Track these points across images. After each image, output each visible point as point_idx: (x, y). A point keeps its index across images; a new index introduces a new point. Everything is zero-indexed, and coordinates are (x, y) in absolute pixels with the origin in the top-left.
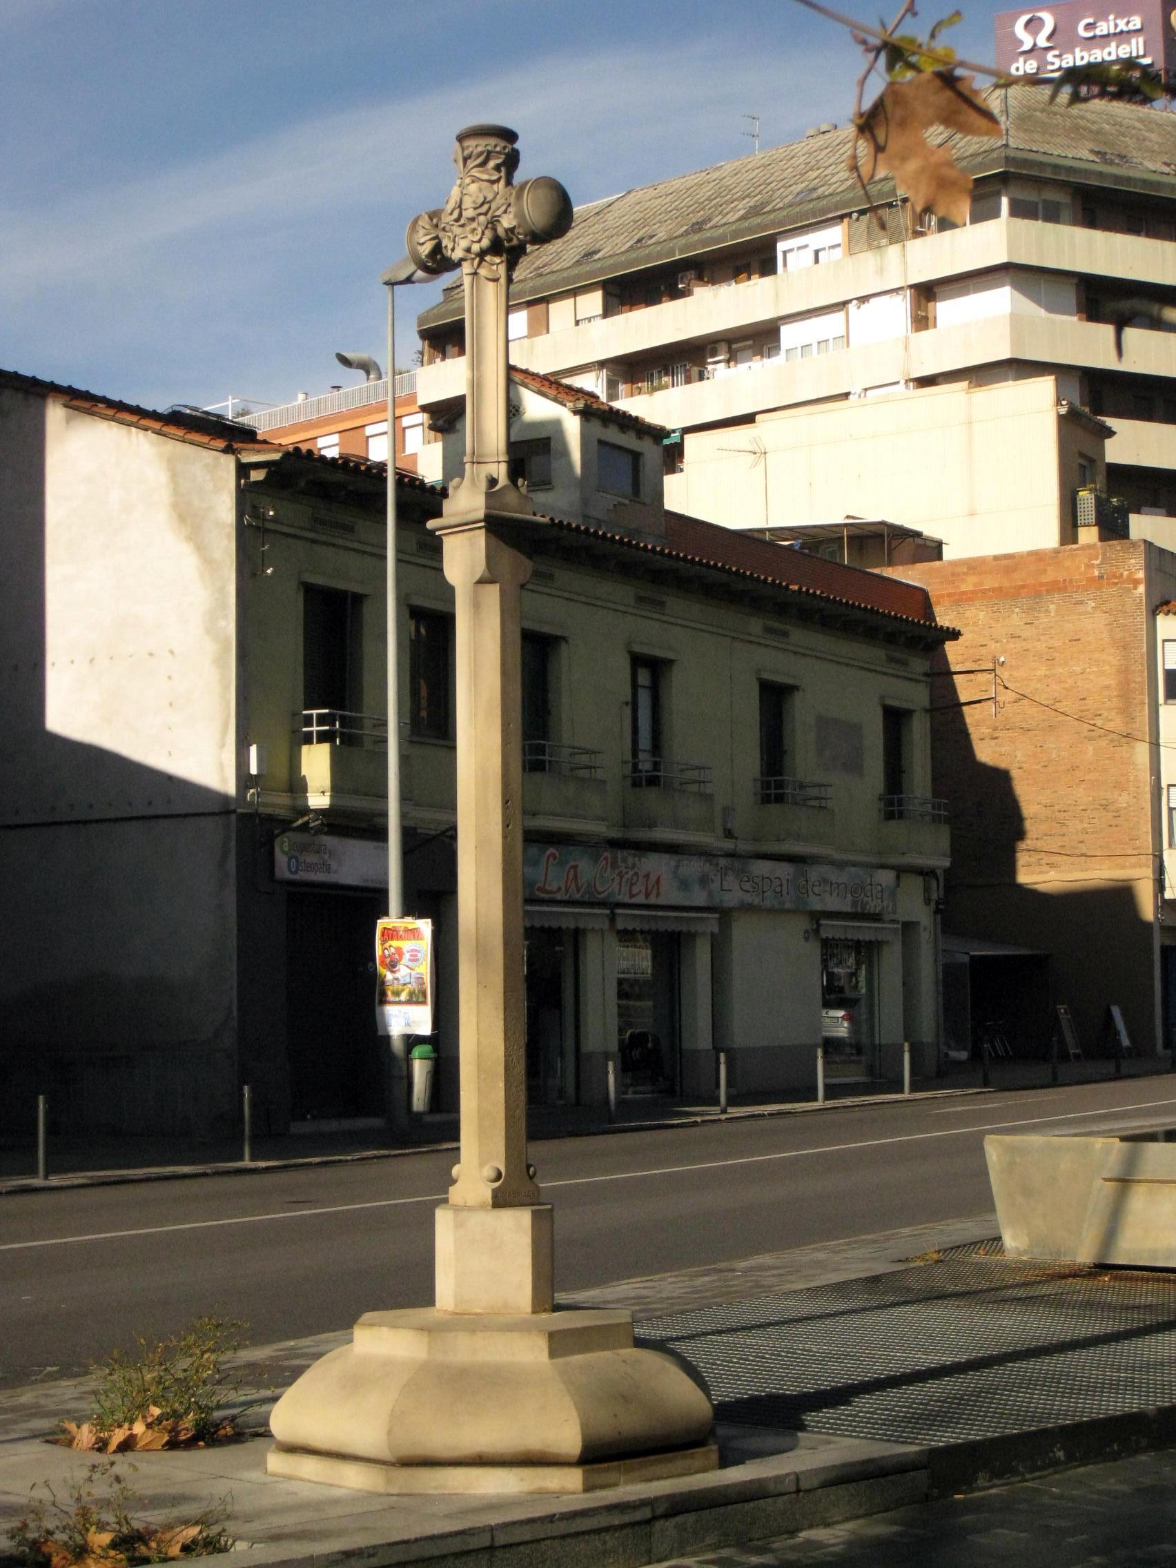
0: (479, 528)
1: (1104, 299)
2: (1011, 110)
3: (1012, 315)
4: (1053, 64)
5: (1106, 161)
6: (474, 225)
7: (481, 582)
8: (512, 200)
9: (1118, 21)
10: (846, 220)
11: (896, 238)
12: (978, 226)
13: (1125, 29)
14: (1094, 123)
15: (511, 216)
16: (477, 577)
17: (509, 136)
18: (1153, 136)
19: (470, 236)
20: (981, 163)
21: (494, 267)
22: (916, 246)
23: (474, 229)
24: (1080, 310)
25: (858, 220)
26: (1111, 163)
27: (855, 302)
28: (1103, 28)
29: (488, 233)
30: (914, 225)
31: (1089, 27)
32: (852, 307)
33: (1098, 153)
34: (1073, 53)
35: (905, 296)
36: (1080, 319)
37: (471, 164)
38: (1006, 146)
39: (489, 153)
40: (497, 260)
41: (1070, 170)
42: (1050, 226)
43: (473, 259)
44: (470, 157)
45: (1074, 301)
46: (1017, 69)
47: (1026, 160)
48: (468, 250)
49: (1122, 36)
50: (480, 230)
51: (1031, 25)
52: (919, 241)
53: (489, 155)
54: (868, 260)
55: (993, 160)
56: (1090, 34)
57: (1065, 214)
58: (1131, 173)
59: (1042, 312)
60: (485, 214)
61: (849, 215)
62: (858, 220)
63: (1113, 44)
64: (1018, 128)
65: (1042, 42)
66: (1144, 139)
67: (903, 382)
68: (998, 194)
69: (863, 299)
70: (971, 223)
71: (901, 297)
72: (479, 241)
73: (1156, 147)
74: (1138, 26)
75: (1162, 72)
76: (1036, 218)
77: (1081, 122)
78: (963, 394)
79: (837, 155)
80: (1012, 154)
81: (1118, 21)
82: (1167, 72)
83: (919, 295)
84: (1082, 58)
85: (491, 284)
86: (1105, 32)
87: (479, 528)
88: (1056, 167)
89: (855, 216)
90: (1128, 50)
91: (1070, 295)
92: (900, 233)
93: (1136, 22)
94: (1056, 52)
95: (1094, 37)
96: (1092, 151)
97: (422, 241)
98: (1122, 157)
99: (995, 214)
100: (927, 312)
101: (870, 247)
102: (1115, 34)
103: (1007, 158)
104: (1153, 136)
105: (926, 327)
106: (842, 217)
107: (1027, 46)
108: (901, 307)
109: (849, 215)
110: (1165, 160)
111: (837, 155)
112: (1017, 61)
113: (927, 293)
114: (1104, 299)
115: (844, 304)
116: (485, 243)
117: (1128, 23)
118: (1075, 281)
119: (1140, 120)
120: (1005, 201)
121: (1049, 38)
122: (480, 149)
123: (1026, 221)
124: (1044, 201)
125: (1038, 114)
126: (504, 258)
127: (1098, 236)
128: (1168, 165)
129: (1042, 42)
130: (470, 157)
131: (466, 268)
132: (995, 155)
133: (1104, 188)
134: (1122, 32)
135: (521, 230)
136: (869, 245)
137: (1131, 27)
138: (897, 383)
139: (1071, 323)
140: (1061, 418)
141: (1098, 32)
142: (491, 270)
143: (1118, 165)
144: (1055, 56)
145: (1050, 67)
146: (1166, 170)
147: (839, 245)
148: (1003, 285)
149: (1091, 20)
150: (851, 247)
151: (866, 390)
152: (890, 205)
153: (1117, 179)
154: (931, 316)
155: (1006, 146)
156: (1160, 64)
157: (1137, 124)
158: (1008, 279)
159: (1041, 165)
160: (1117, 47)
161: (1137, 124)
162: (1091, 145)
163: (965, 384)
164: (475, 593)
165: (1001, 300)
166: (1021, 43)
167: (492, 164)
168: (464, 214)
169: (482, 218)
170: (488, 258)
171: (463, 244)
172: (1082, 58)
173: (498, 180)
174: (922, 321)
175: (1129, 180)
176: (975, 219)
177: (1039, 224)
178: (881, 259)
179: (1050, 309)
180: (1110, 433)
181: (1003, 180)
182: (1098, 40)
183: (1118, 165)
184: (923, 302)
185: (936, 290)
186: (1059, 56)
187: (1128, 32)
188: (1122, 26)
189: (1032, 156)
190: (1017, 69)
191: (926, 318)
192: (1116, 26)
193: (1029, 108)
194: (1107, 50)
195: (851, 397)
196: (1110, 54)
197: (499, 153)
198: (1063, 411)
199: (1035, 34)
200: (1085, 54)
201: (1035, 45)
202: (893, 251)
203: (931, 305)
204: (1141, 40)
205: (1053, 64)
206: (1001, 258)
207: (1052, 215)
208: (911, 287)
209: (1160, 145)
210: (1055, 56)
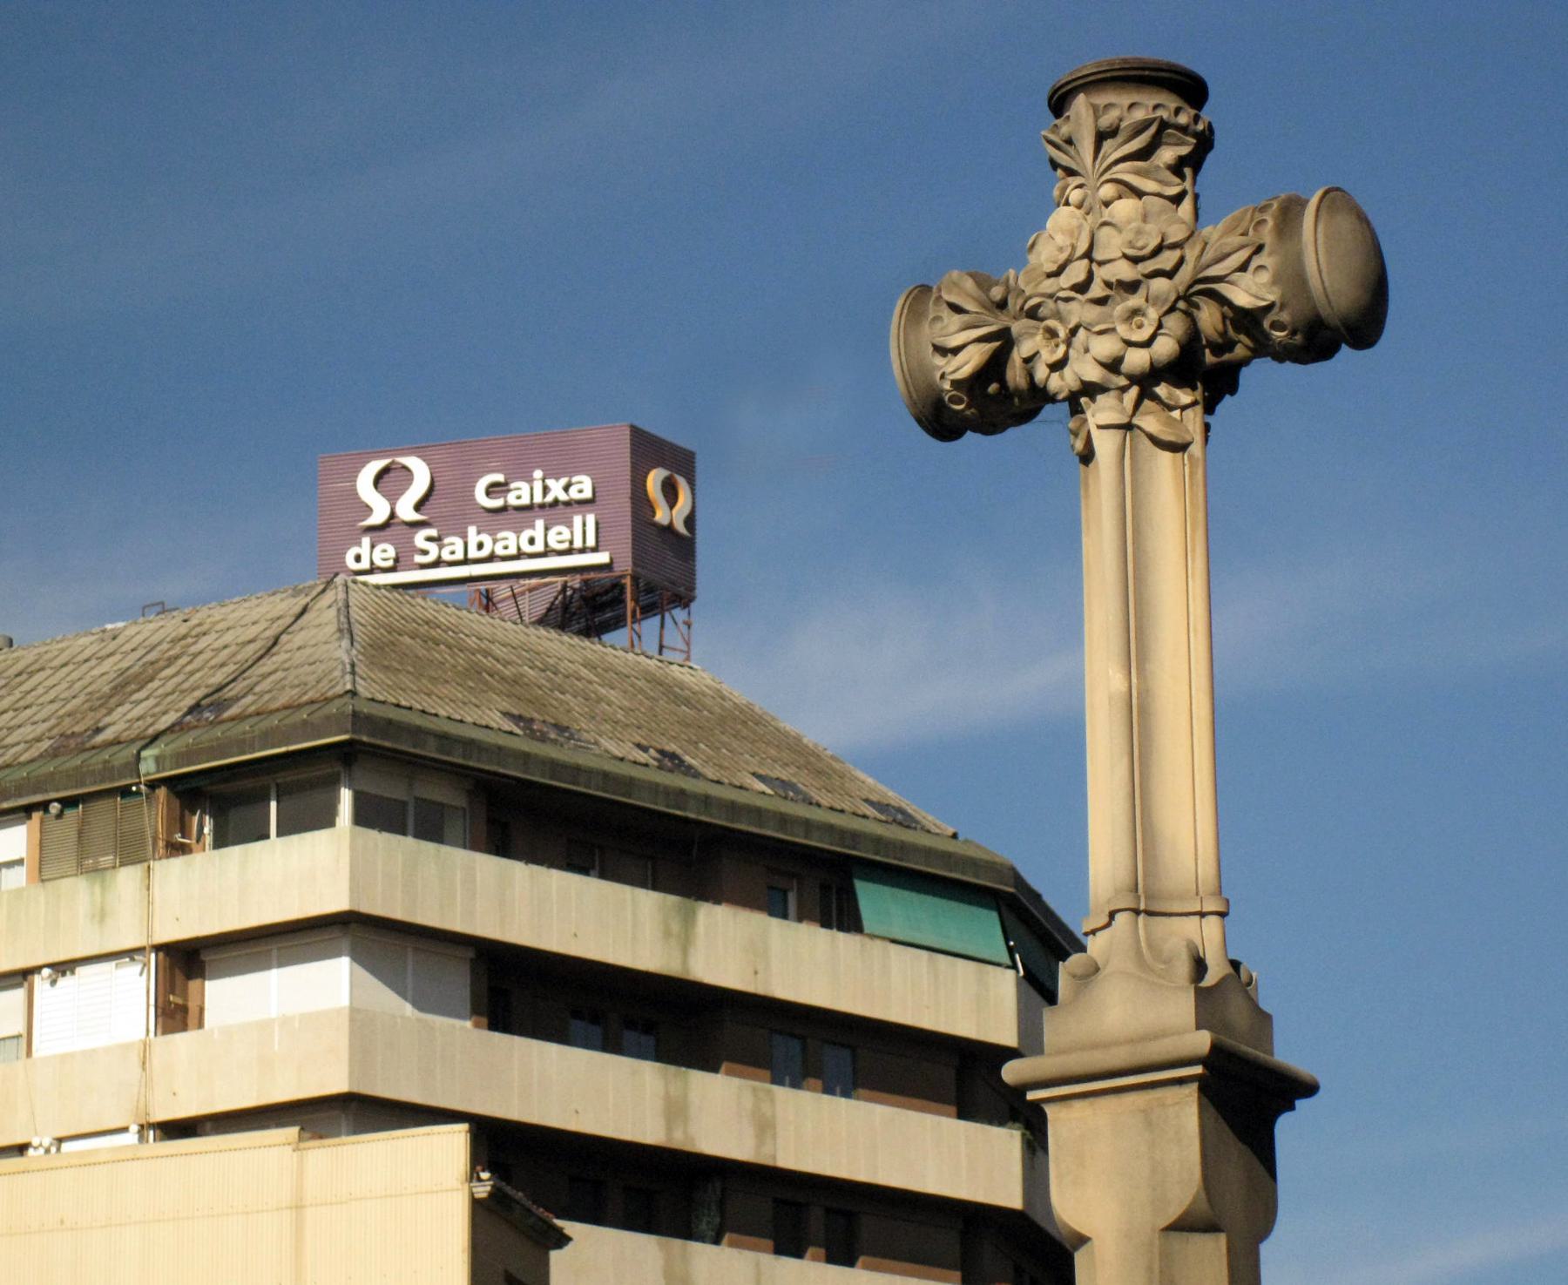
0: (1180, 1081)
1: (522, 990)
2: (357, 629)
3: (354, 1011)
4: (425, 553)
5: (532, 735)
6: (1135, 301)
7: (1185, 1225)
8: (1267, 235)
9: (550, 482)
10: (37, 816)
11: (131, 852)
12: (295, 839)
13: (563, 497)
14: (506, 663)
15: (1264, 277)
16: (1173, 1213)
17: (1192, 89)
18: (613, 695)
19: (1122, 330)
20: (305, 722)
21: (1176, 414)
22: (171, 872)
23: (1135, 312)
24: (476, 1011)
25: (60, 816)
26: (543, 739)
27: (46, 972)
28: (520, 493)
29: (1175, 324)
30: (170, 833)
31: (492, 490)
32: (40, 982)
33: (516, 719)
34: (464, 536)
35: (146, 965)
36: (477, 1025)
37: (1113, 150)
38: (353, 693)
39: (1164, 125)
40: (1185, 397)
41: (470, 745)
42: (429, 847)
43: (1124, 389)
44: (1112, 133)
45: (466, 993)
46: (358, 559)
47: (390, 722)
48: (1113, 365)
49: (556, 510)
50: (1153, 314)
51: (386, 478)
52: (177, 863)
53: (1162, 132)
54: (77, 891)
55: (328, 718)
56: (497, 503)
57: (455, 826)
58: (582, 760)
59: (408, 1009)
60: (1169, 274)
61: (44, 806)
62: (60, 816)
63: (540, 524)
64: (372, 663)
65: (406, 512)
66: (600, 700)
67: (134, 1128)
68: (332, 784)
69: (63, 968)
70: (279, 834)
71: (137, 968)
72: (1148, 344)
73: (620, 716)
74: (588, 494)
75: (628, 581)
76: (402, 831)
77: (488, 662)
78: (289, 1149)
79: (17, 694)
80: (366, 709)
81: (550, 482)
82: (635, 579)
83: (172, 968)
84: (480, 546)
85: (1166, 457)
86: (525, 501)
87: (1180, 1081)
88: (443, 737)
89: (55, 808)
90: (566, 535)
91: (459, 979)
92: (143, 844)
93: (583, 486)
94: (433, 532)
95: (504, 509)
96: (506, 714)
97: (954, 341)
98: (560, 728)
99: (326, 819)
100: (186, 999)
101: (81, 870)
102: (542, 506)
103: (355, 714)
104: (613, 695)
105: (184, 1027)
106: (28, 810)
107: (379, 516)
108: (134, 987)
109: (44, 806)
110: (638, 739)
111: (17, 694)
112: (359, 544)
113: (186, 963)
114: (522, 990)
115: (23, 976)
116: (1166, 347)
117: (566, 489)
118: (471, 954)
119: (587, 664)
120: (346, 797)
121: (418, 507)
122: (1139, 115)
123: (386, 835)
124: (417, 799)
125: (407, 640)
126: (1198, 394)
127: (519, 872)
128: (645, 749)
129: (406, 512)
130: (1112, 133)
131: (1102, 411)
132: (332, 709)
133: (531, 784)
134: (556, 502)
135: (1285, 317)
136: (80, 864)
137: (574, 494)
138: (125, 1130)
139: (462, 1033)
140: (476, 1204)
141: (512, 500)
142: (1171, 422)
143: (554, 742)
144: (429, 539)
145: (419, 559)
146: (642, 757)
147: (20, 862)
148: (339, 955)
149: (500, 478)
150: (44, 866)
151: (60, 1140)
152: (125, 792)
153: (555, 767)
154: (192, 1005)
155: (353, 693)
156: (625, 565)
157: (584, 672)
158: (345, 943)
159: (417, 733)
160: (547, 529)
161: (584, 672)
162: (506, 705)
163: (293, 1132)
164: (1166, 1256)
165: (330, 982)
166: (368, 510)
167: (1167, 155)
168: (1101, 273)
169: (1160, 284)
170: (1162, 390)
171: (1105, 347)
172: (480, 546)
173: (1177, 200)
174: (175, 1015)
175: (576, 771)
176: (221, 841)
177: (409, 842)
178: (103, 889)
179: (421, 1004)
180: (562, 1240)
181: (346, 756)
182: (512, 514)
183: (554, 742)
184: (179, 977)
185: (206, 957)
186: (436, 539)
187: (568, 504)
188: (557, 490)
189: (394, 714)
190: (358, 559)
191: (184, 1009)
192: (546, 490)
193: (391, 630)
194: (527, 534)
195: (31, 1152)
196: (532, 541)
197: (1184, 129)
198: (482, 1191)
199: (392, 497)
200: (486, 539)
201: (393, 515)
202: (127, 879)
203: (193, 985)
204: (591, 519)
205: (425, 553)
206: (337, 902)
207: (431, 828)
208: (158, 948)
209: (627, 711)
210: (429, 539)
